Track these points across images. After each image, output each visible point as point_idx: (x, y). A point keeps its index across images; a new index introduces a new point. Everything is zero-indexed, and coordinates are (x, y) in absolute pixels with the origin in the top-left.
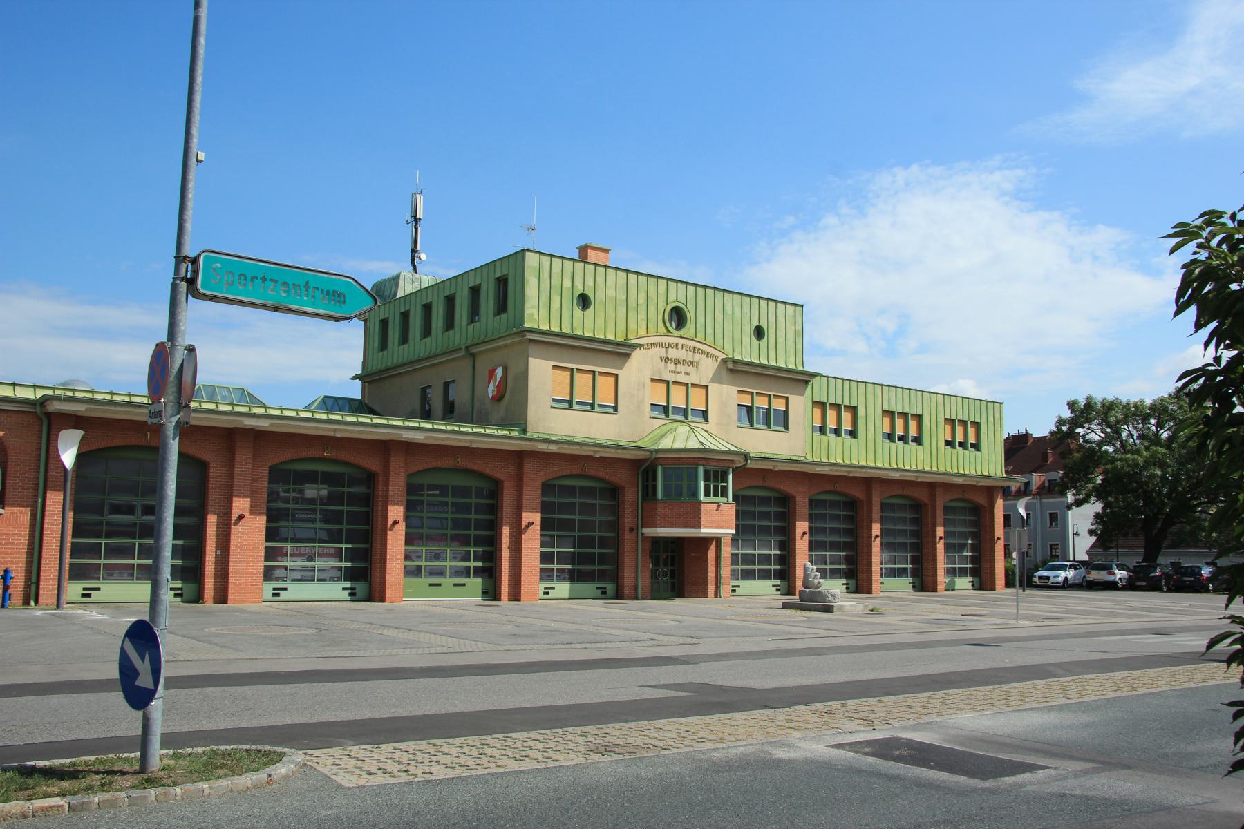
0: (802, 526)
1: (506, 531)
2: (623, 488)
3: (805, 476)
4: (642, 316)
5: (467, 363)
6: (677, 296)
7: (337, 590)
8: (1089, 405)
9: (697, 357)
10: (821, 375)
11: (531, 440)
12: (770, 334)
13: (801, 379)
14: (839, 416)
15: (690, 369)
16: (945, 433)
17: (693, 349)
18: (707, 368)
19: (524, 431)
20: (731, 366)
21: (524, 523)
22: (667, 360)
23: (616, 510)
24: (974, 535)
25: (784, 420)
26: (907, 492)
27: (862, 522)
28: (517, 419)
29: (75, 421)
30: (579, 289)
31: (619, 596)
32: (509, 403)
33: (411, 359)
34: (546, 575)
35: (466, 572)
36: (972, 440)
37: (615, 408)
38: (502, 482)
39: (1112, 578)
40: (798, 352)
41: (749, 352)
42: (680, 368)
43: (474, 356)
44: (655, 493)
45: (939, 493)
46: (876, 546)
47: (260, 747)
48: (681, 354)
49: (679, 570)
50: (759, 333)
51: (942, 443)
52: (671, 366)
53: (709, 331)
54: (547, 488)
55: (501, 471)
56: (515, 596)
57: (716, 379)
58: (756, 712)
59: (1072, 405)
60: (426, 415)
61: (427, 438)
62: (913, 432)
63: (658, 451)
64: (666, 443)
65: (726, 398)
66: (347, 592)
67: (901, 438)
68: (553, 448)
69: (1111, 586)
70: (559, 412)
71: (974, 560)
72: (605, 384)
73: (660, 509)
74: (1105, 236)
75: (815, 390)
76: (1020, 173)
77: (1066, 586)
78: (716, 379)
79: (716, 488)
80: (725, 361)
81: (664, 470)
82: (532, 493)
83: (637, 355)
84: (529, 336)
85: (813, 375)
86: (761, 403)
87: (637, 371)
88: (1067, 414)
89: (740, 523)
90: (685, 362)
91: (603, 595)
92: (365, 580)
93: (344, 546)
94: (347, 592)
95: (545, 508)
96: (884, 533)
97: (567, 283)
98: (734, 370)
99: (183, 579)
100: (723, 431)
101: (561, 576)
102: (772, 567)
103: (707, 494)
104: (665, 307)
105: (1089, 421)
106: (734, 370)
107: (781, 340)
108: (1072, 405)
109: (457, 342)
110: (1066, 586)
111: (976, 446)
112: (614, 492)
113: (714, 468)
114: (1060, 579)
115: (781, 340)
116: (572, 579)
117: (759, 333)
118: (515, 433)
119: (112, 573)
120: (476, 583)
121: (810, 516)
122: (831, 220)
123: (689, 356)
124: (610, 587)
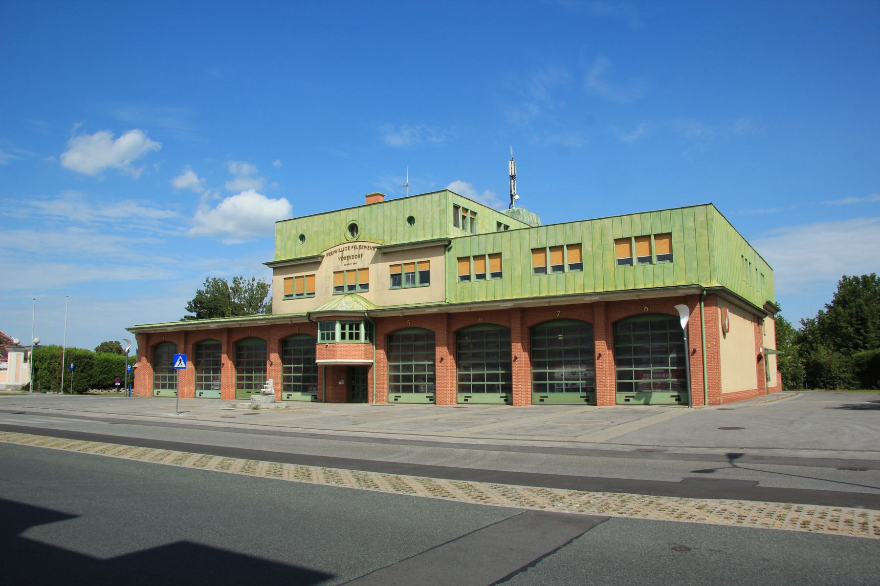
9: (361, 251)
15: (355, 260)
18: (369, 255)
22: (342, 258)
25: (425, 278)
30: (301, 233)
42: (351, 261)
48: (352, 252)
52: (345, 262)
57: (375, 260)
58: (728, 501)
66: (583, 399)
78: (375, 260)
79: (328, 334)
83: (325, 261)
90: (354, 257)
94: (583, 399)
98: (385, 252)
101: (296, 389)
103: (323, 338)
104: (345, 227)
106: (385, 252)
123: (357, 252)
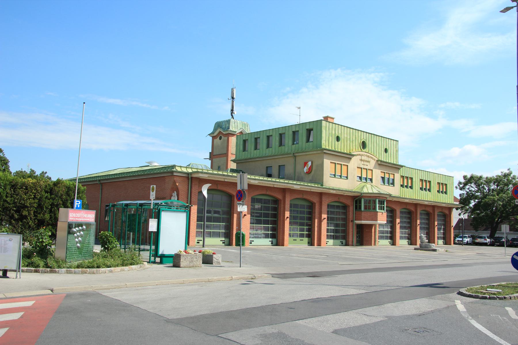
0: (398, 221)
1: (316, 220)
2: (349, 206)
3: (400, 203)
4: (354, 144)
5: (292, 160)
6: (364, 137)
7: (267, 242)
8: (472, 177)
9: (370, 159)
10: (405, 167)
11: (324, 188)
12: (389, 151)
13: (397, 167)
14: (408, 183)
15: (368, 164)
16: (437, 189)
17: (368, 156)
19: (322, 185)
20: (379, 163)
21: (322, 218)
22: (361, 160)
23: (345, 214)
24: (444, 225)
26: (408, 207)
27: (419, 220)
28: (320, 180)
29: (206, 181)
31: (347, 244)
32: (315, 174)
33: (264, 155)
34: (328, 237)
35: (302, 236)
36: (410, 185)
37: (347, 177)
38: (315, 203)
39: (486, 241)
40: (397, 158)
41: (384, 158)
42: (365, 163)
43: (295, 156)
44: (360, 208)
45: (436, 209)
46: (287, 222)
47: (494, 284)
49: (363, 236)
50: (386, 151)
51: (436, 191)
52: (363, 162)
53: (372, 150)
54: (329, 206)
55: (315, 200)
56: (319, 244)
57: (375, 168)
59: (465, 177)
60: (269, 176)
61: (301, 188)
62: (428, 188)
63: (364, 193)
64: (365, 190)
65: (377, 174)
67: (406, 186)
68: (334, 192)
69: (485, 244)
70: (339, 180)
71: (444, 234)
72: (344, 168)
73: (363, 214)
74: (415, 102)
75: (402, 172)
76: (382, 74)
77: (467, 244)
78: (375, 168)
80: (377, 161)
81: (364, 200)
82: (325, 208)
83: (354, 159)
84: (325, 151)
85: (402, 166)
86: (387, 176)
87: (354, 163)
88: (463, 181)
89: (292, 215)
90: (366, 161)
91: (342, 244)
92: (275, 238)
93: (270, 226)
95: (328, 213)
96: (291, 217)
97: (333, 132)
98: (381, 164)
99: (225, 237)
100: (375, 187)
102: (221, 231)
105: (471, 183)
106: (381, 164)
107: (392, 153)
108: (465, 177)
109: (286, 150)
110: (467, 244)
111: (446, 193)
112: (345, 207)
113: (382, 200)
114: (466, 242)
115: (392, 153)
116: (333, 239)
117: (386, 151)
118: (319, 186)
119: (210, 235)
120: (306, 240)
121: (328, 211)
122: (304, 90)
124: (344, 241)
